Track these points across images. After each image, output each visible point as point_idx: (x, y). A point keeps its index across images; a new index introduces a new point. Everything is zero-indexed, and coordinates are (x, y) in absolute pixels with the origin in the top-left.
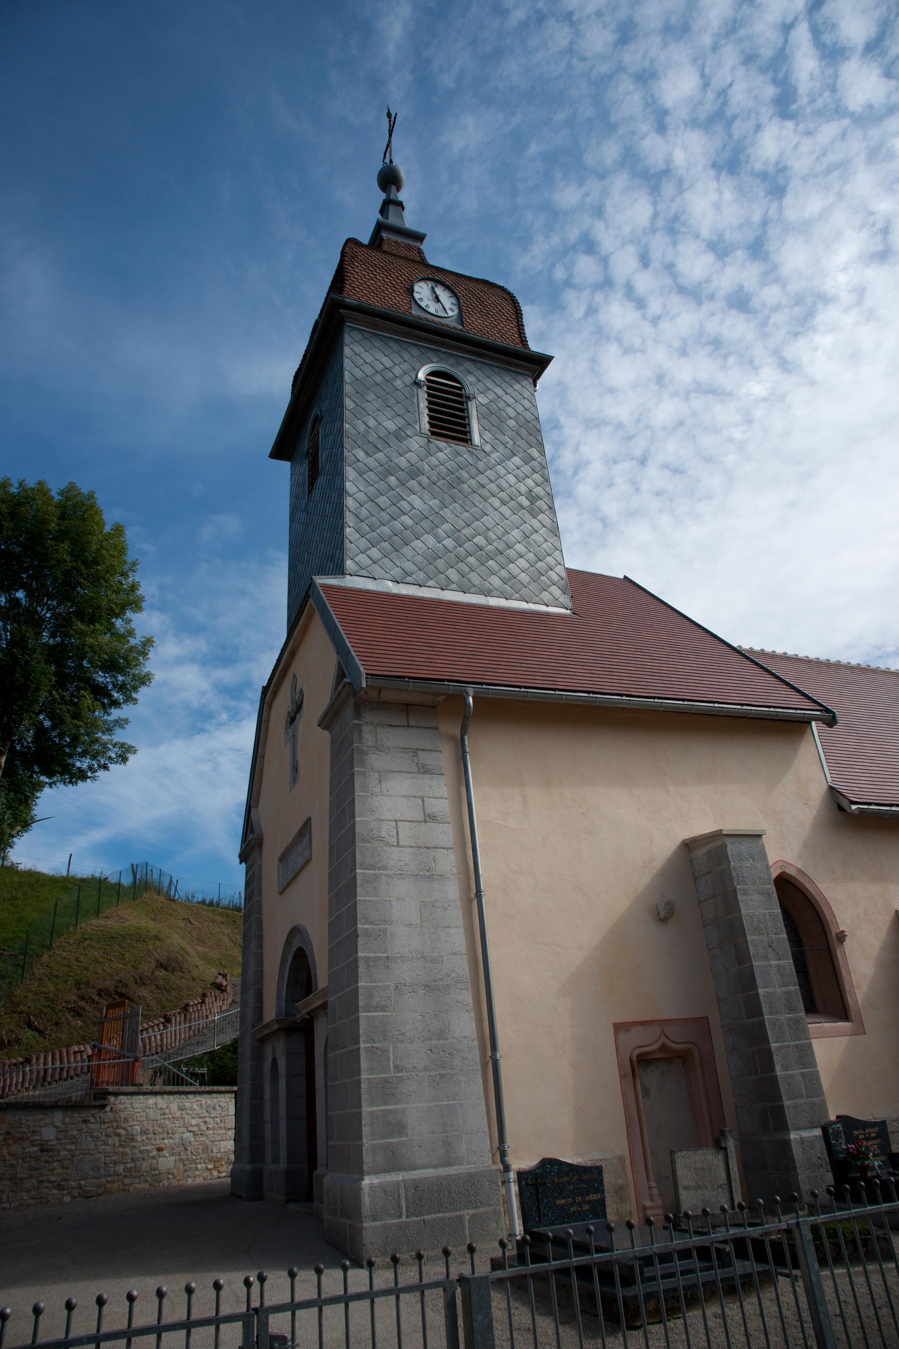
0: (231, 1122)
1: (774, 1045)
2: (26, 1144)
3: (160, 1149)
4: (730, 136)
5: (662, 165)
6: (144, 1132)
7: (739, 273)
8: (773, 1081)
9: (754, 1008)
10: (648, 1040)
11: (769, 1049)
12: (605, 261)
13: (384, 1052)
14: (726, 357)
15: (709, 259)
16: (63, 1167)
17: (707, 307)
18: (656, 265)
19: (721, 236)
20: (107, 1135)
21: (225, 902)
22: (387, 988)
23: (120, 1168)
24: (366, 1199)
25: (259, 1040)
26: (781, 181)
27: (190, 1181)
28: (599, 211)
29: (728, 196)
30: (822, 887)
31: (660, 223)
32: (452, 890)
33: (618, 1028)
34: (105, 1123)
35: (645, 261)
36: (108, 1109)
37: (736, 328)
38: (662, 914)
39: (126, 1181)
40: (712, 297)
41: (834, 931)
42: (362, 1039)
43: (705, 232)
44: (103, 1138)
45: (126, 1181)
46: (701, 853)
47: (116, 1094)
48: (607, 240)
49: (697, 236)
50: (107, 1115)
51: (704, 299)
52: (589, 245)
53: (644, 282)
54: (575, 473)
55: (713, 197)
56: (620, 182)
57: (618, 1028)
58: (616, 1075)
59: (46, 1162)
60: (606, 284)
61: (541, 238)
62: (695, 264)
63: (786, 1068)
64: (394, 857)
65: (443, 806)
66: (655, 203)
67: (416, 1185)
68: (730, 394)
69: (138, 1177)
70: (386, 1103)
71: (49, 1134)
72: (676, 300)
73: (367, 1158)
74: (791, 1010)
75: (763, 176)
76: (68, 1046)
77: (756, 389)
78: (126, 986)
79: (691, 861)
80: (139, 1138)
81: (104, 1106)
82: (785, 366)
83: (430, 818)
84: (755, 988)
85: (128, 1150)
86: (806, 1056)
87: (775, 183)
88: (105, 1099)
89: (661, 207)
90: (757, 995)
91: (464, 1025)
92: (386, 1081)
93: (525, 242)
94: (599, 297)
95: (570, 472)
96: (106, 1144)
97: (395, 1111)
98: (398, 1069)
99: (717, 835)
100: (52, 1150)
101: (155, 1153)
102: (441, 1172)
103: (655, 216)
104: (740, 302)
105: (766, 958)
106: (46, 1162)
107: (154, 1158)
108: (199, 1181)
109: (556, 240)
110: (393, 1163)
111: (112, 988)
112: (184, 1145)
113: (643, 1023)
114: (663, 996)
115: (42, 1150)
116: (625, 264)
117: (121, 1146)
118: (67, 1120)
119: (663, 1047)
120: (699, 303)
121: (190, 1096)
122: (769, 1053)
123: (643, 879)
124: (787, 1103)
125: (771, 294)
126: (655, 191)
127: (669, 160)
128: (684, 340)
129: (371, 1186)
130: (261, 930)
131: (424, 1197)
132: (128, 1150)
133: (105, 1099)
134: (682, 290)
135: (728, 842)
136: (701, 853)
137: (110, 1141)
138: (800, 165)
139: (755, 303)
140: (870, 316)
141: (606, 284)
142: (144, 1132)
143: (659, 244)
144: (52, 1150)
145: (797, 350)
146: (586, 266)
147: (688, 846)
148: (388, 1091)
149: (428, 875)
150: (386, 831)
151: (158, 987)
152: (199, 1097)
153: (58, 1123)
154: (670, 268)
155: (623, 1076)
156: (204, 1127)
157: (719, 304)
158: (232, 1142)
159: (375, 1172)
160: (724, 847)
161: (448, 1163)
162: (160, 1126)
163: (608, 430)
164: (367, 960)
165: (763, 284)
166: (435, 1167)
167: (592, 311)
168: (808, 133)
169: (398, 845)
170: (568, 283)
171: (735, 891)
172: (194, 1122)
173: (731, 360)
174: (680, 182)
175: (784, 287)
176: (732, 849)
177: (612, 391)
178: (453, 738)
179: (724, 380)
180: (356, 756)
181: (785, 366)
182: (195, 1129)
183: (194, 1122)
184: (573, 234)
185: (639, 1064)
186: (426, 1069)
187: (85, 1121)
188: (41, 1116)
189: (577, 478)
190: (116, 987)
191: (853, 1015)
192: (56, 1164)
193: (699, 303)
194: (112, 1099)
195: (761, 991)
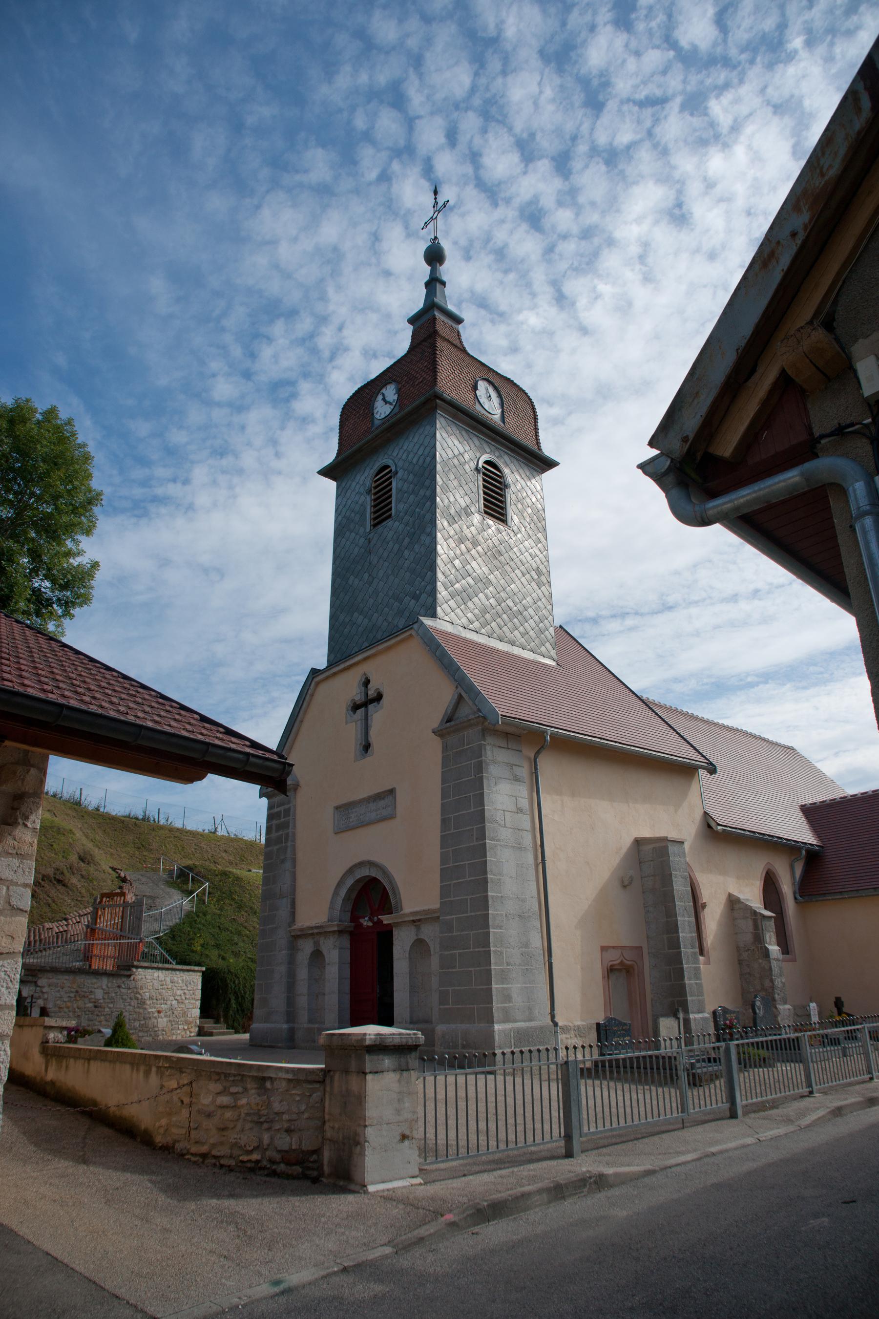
0: (199, 996)
1: (685, 966)
2: (86, 1000)
3: (159, 1012)
4: (564, 24)
5: (492, 31)
6: (151, 998)
7: (538, 184)
8: (683, 987)
9: (675, 944)
10: (614, 957)
11: (682, 968)
12: (410, 123)
13: (501, 953)
14: (506, 272)
15: (514, 158)
16: (106, 1020)
17: (501, 211)
18: (462, 146)
19: (532, 135)
20: (131, 999)
21: (66, 796)
22: (502, 915)
23: (137, 1024)
24: (497, 1037)
25: (293, 936)
26: (601, 98)
27: (174, 1038)
28: (417, 61)
29: (548, 93)
30: (697, 874)
31: (477, 101)
32: (529, 858)
33: (604, 949)
34: (129, 988)
35: (452, 136)
36: (132, 978)
37: (526, 245)
38: (626, 883)
39: (141, 1034)
40: (508, 201)
41: (701, 902)
42: (491, 945)
43: (519, 126)
44: (129, 1000)
45: (141, 1034)
46: (648, 848)
47: (137, 967)
48: (416, 99)
49: (510, 129)
50: (132, 984)
51: (500, 202)
52: (395, 97)
53: (446, 164)
54: (332, 358)
55: (534, 88)
56: (446, 34)
57: (604, 949)
58: (601, 976)
59: (98, 1015)
60: (405, 151)
61: (348, 68)
62: (501, 162)
63: (690, 979)
64: (505, 834)
65: (524, 803)
66: (476, 74)
67: (518, 1031)
68: (501, 315)
69: (147, 1032)
70: (503, 983)
71: (99, 994)
72: (471, 192)
73: (495, 1014)
74: (693, 947)
75: (584, 82)
76: (42, 923)
77: (533, 320)
78: (62, 873)
79: (639, 851)
80: (148, 1002)
81: (130, 976)
82: (561, 299)
83: (520, 810)
84: (678, 932)
85: (141, 1011)
86: (697, 973)
87: (594, 96)
88: (130, 970)
89: (483, 81)
90: (678, 937)
91: (537, 942)
92: (503, 971)
93: (330, 70)
94: (396, 166)
95: (327, 354)
96: (130, 1005)
97: (507, 989)
98: (508, 964)
99: (665, 839)
100: (101, 1007)
101: (156, 1014)
102: (527, 1024)
103: (473, 90)
104: (533, 217)
105: (683, 916)
106: (98, 1015)
107: (155, 1018)
108: (179, 1037)
109: (364, 78)
110: (507, 1019)
111: (52, 876)
112: (171, 1009)
113: (614, 947)
114: (624, 933)
115: (96, 1007)
116: (431, 135)
117: (138, 1007)
118: (109, 985)
119: (622, 963)
120: (495, 204)
121: (178, 973)
122: (682, 969)
123: (615, 860)
124: (689, 998)
125: (563, 218)
126: (479, 62)
127: (500, 26)
128: (471, 242)
129: (499, 1030)
130: (295, 854)
131: (522, 1036)
132: (141, 1011)
133: (130, 970)
134: (481, 184)
135: (669, 844)
136: (648, 848)
137: (132, 1004)
138: (622, 86)
139: (546, 223)
140: (647, 279)
141: (405, 151)
142: (151, 998)
143: (470, 122)
144: (101, 1007)
145: (575, 286)
146: (388, 123)
147: (639, 842)
148: (504, 977)
149: (520, 848)
150: (499, 816)
151: (82, 877)
152: (182, 974)
153: (104, 987)
154: (474, 157)
155: (604, 977)
156: (183, 998)
157: (511, 213)
158: (199, 1010)
159: (499, 1022)
160: (666, 848)
161: (530, 1020)
162: (160, 994)
163: (374, 317)
164: (493, 897)
165: (560, 204)
166: (525, 1021)
167: (385, 177)
168: (638, 54)
169: (505, 826)
170: (368, 137)
171: (671, 875)
172: (179, 992)
173: (512, 276)
174: (506, 60)
175: (577, 215)
176: (672, 849)
177: (387, 274)
178: (529, 759)
179: (503, 299)
180: (484, 765)
181: (561, 299)
182: (178, 998)
183: (179, 992)
184: (383, 78)
185: (611, 971)
186: (520, 965)
187: (119, 987)
188: (95, 980)
189: (334, 363)
190: (55, 874)
191: (705, 953)
192: (102, 1017)
193: (495, 204)
194: (134, 970)
195: (681, 935)
